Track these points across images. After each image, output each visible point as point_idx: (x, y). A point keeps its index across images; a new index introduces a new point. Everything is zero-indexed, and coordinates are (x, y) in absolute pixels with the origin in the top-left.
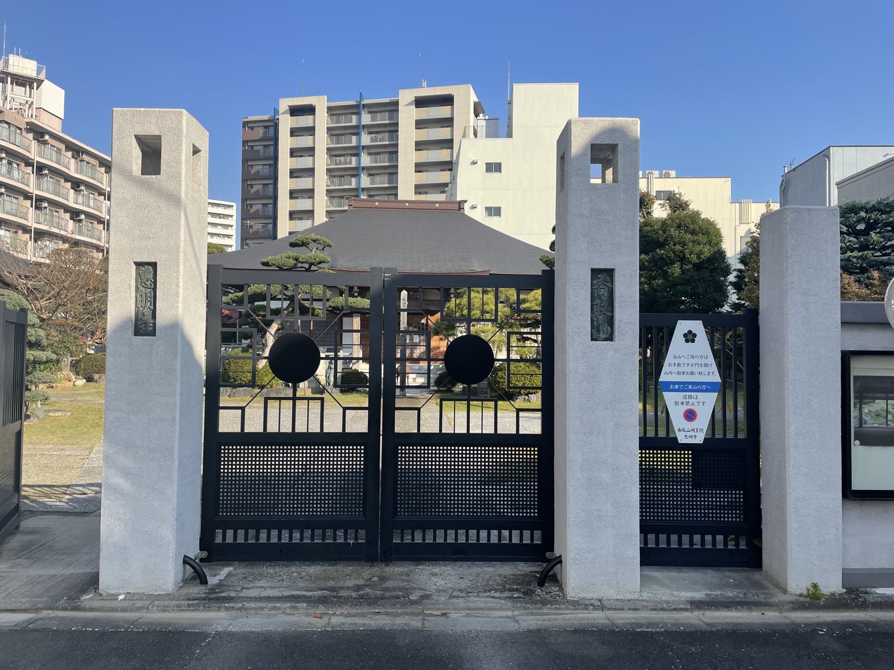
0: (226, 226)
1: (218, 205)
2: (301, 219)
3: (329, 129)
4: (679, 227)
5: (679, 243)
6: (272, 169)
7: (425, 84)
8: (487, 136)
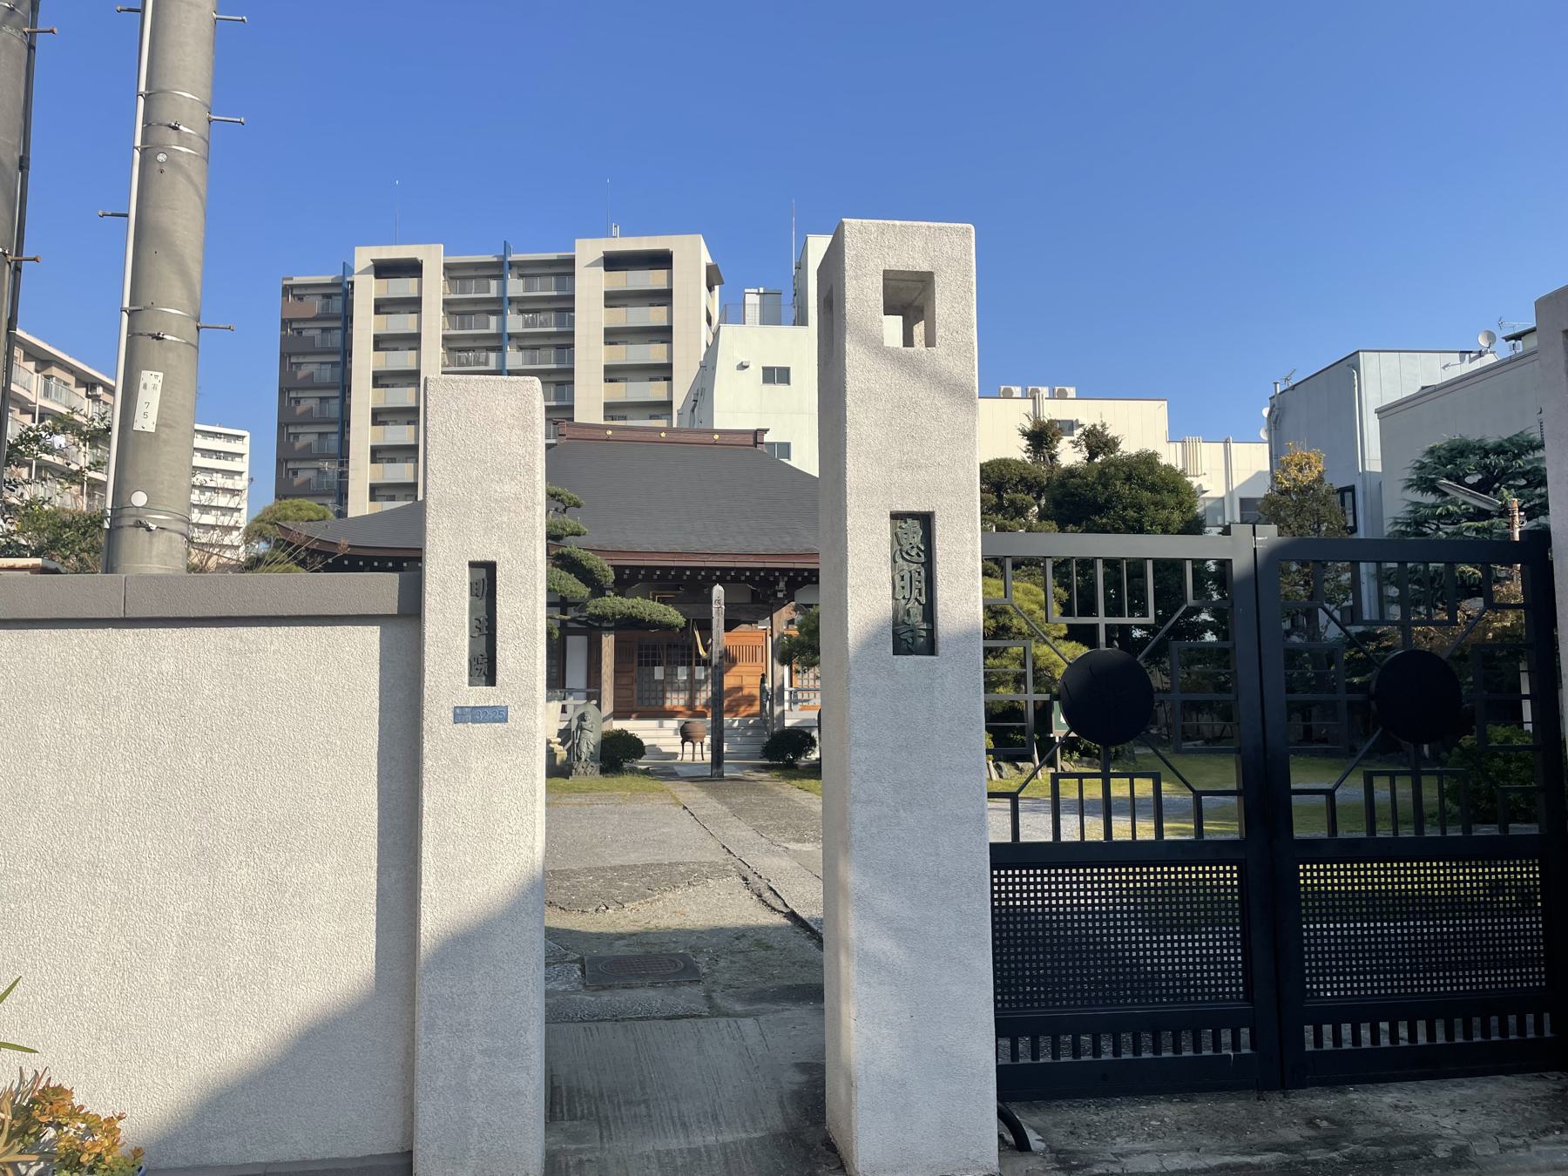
0: (230, 474)
2: (393, 461)
3: (446, 303)
4: (1129, 478)
6: (338, 370)
7: (616, 230)
8: (763, 322)
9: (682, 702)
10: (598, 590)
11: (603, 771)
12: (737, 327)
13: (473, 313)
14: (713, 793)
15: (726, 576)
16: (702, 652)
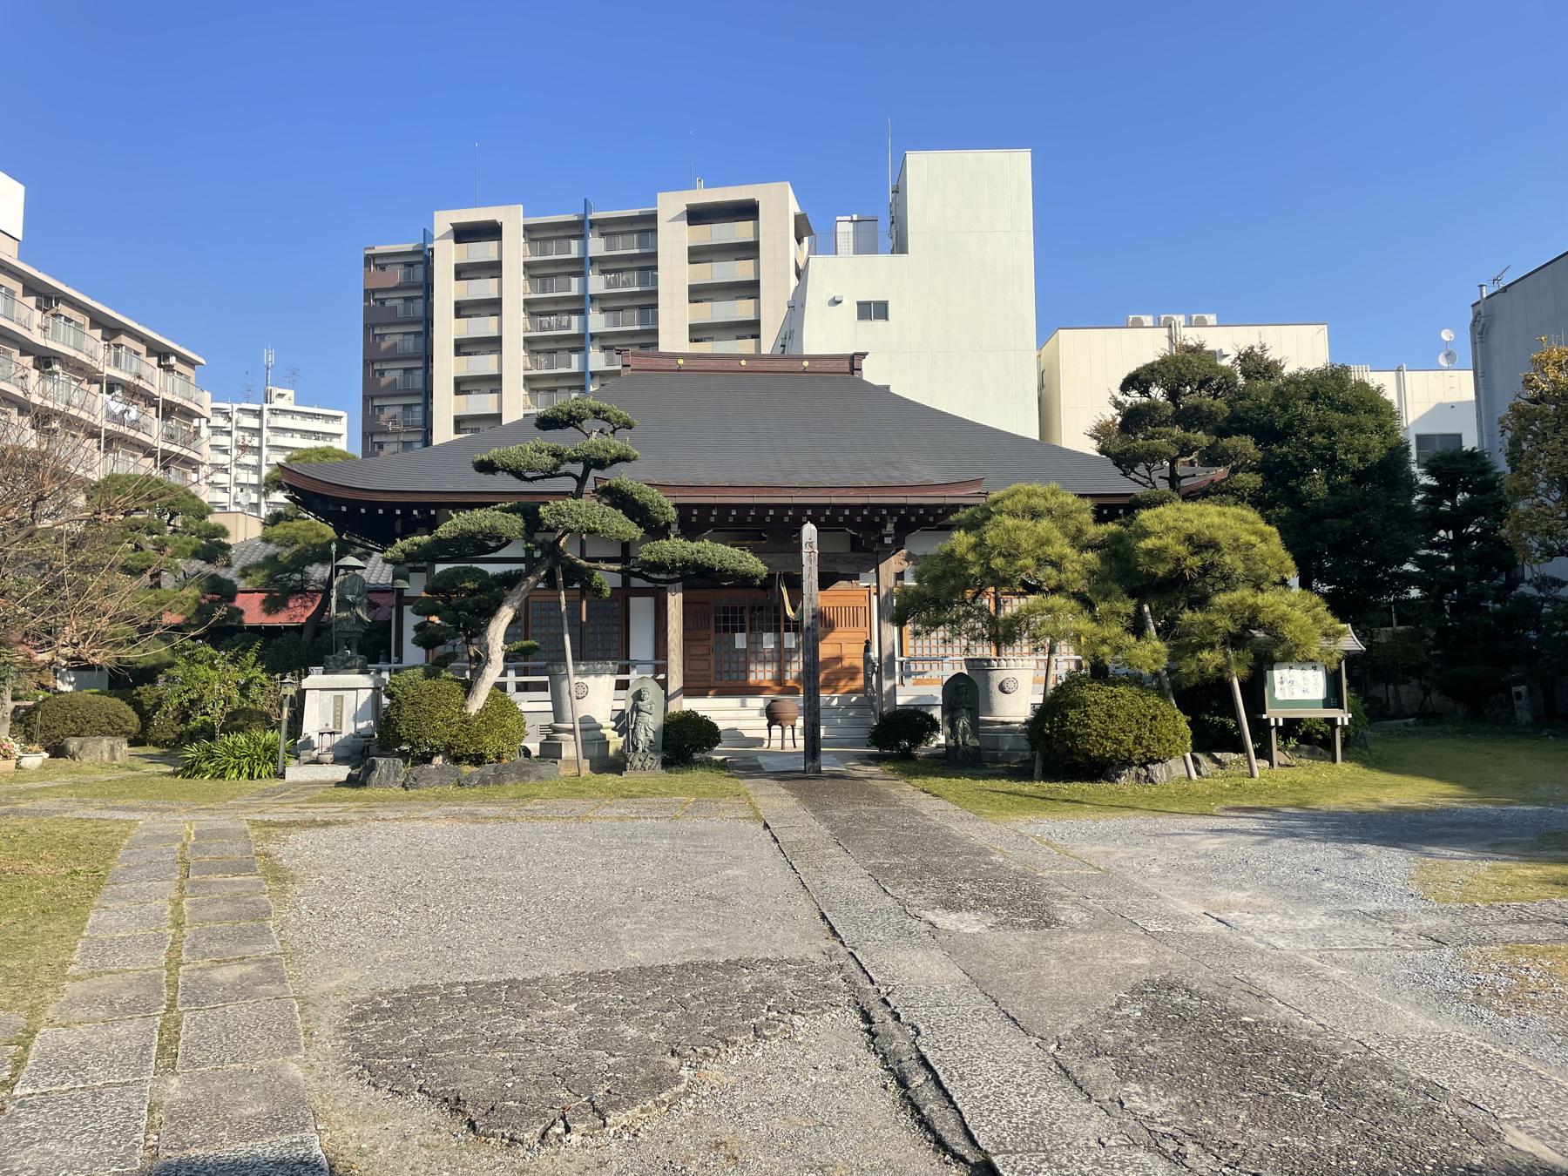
1: (315, 416)
3: (527, 266)
4: (1313, 397)
5: (1320, 430)
6: (421, 340)
8: (857, 251)
9: (769, 676)
10: (656, 530)
11: (666, 764)
12: (829, 259)
13: (555, 275)
14: (807, 799)
15: (817, 514)
16: (790, 612)
